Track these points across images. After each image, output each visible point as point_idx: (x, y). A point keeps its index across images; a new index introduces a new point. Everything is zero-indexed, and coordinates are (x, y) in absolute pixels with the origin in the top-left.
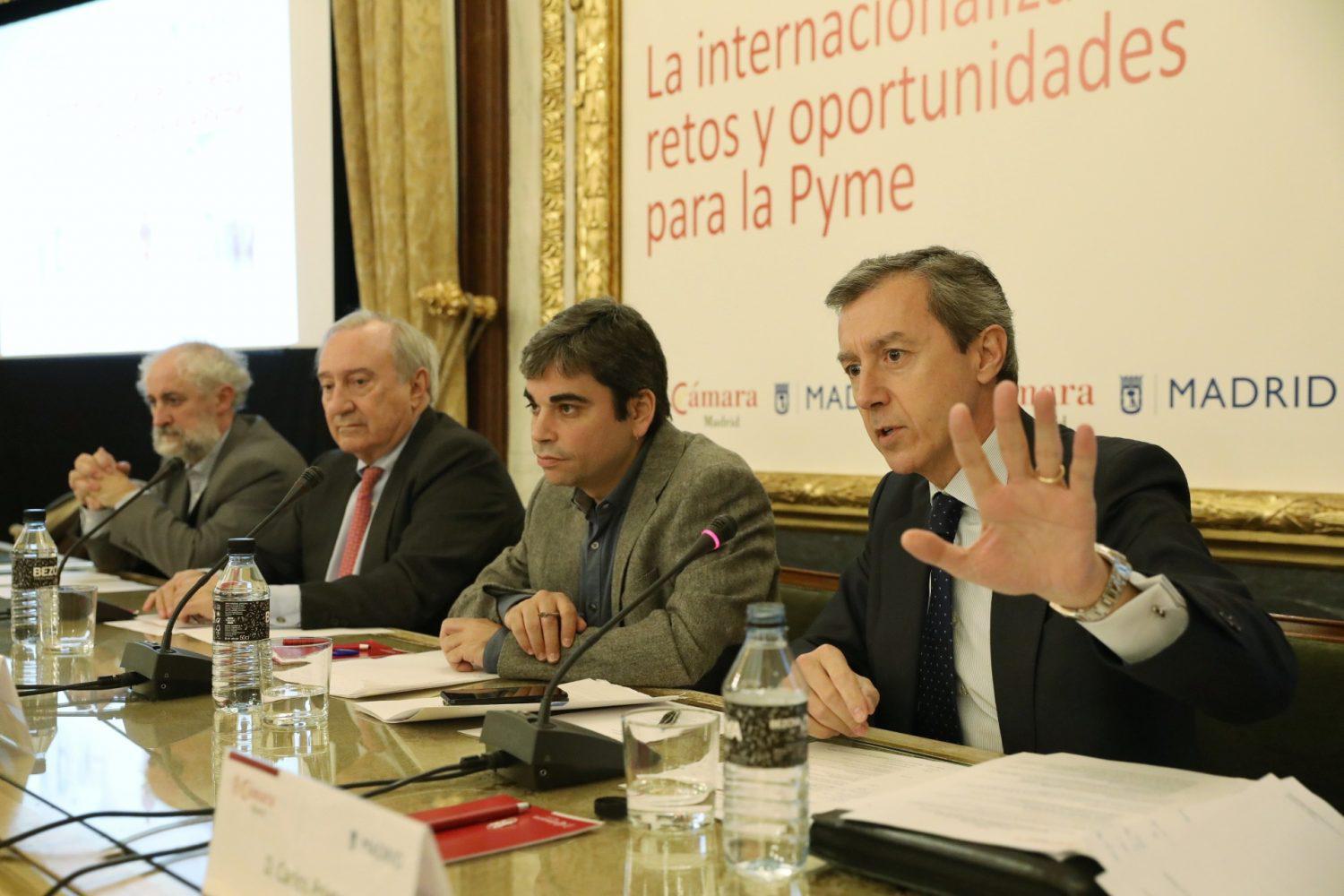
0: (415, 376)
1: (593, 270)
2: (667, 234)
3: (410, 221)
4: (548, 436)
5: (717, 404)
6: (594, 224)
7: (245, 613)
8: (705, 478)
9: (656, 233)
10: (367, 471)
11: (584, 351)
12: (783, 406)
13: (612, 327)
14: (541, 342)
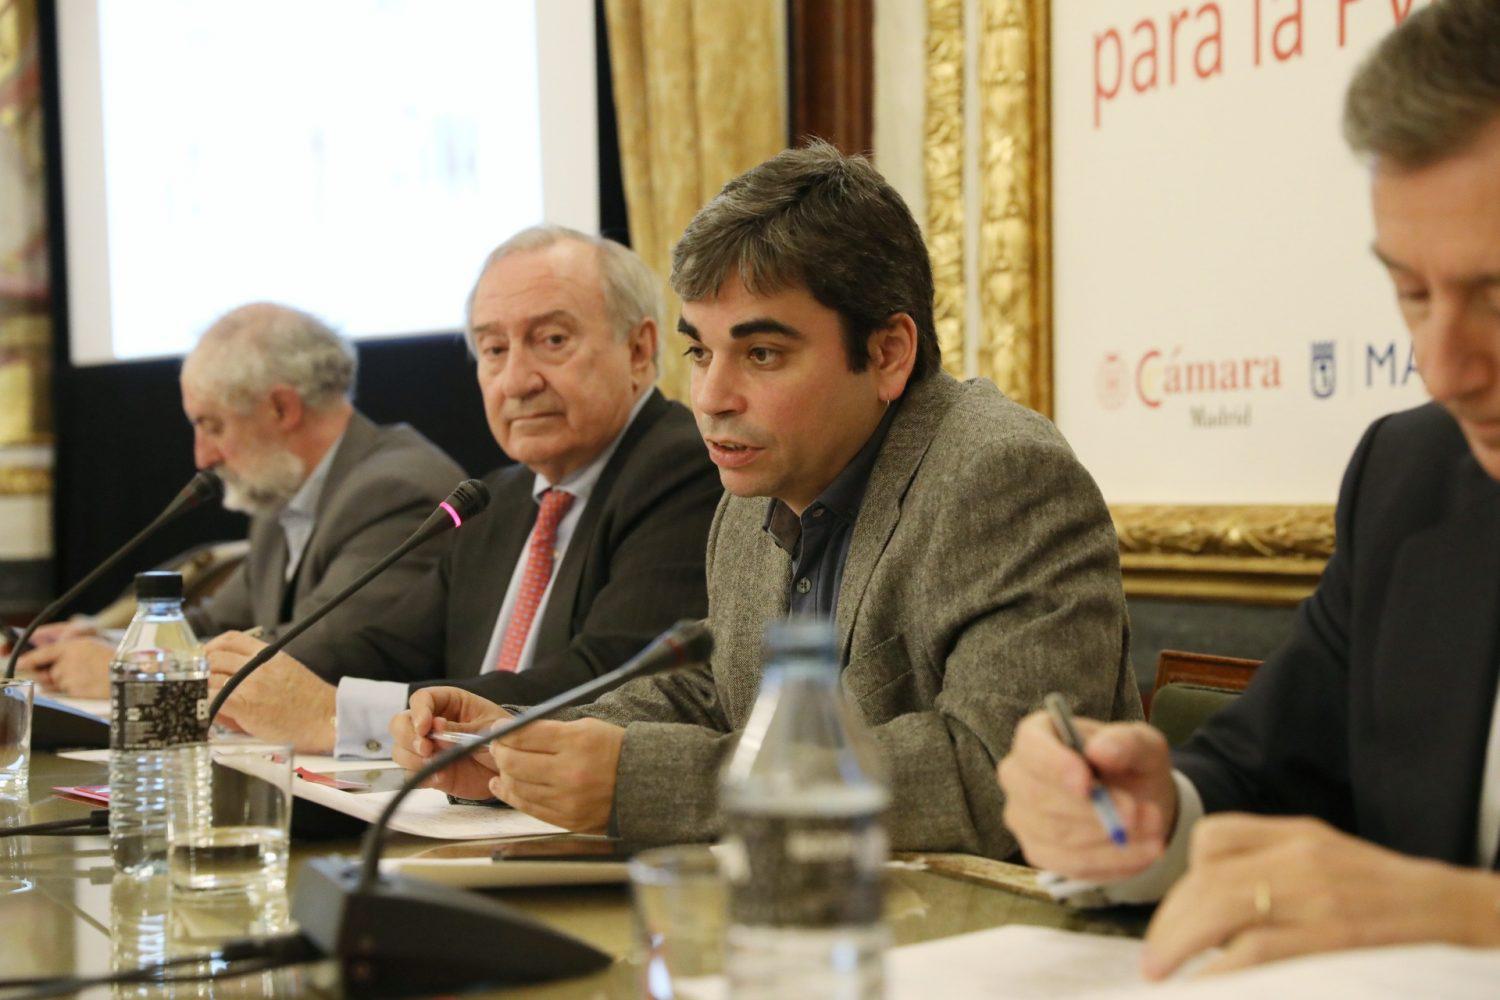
0: (637, 332)
1: (999, 160)
2: (1126, 88)
3: (703, 91)
4: (729, 404)
5: (1213, 386)
6: (1000, 76)
7: (157, 703)
8: (979, 465)
9: (1108, 84)
10: (548, 498)
11: (790, 245)
12: (1325, 381)
13: (837, 203)
14: (710, 233)
